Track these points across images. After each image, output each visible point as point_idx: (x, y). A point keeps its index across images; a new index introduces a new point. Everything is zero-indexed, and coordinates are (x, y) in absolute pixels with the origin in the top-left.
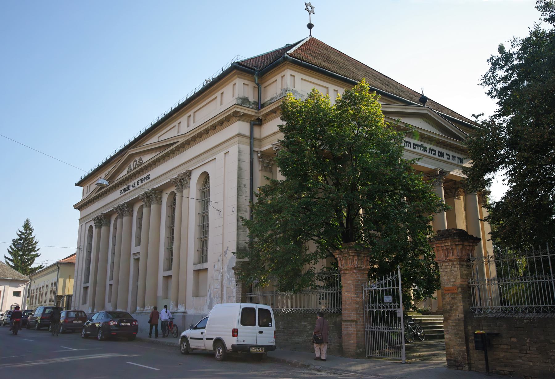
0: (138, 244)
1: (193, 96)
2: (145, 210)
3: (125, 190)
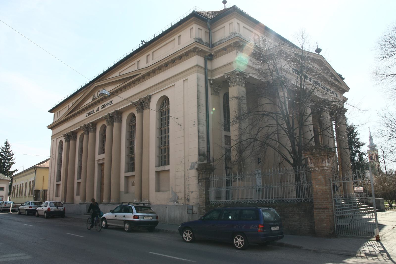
0: (102, 151)
1: (130, 54)
2: (85, 136)
3: (90, 113)
